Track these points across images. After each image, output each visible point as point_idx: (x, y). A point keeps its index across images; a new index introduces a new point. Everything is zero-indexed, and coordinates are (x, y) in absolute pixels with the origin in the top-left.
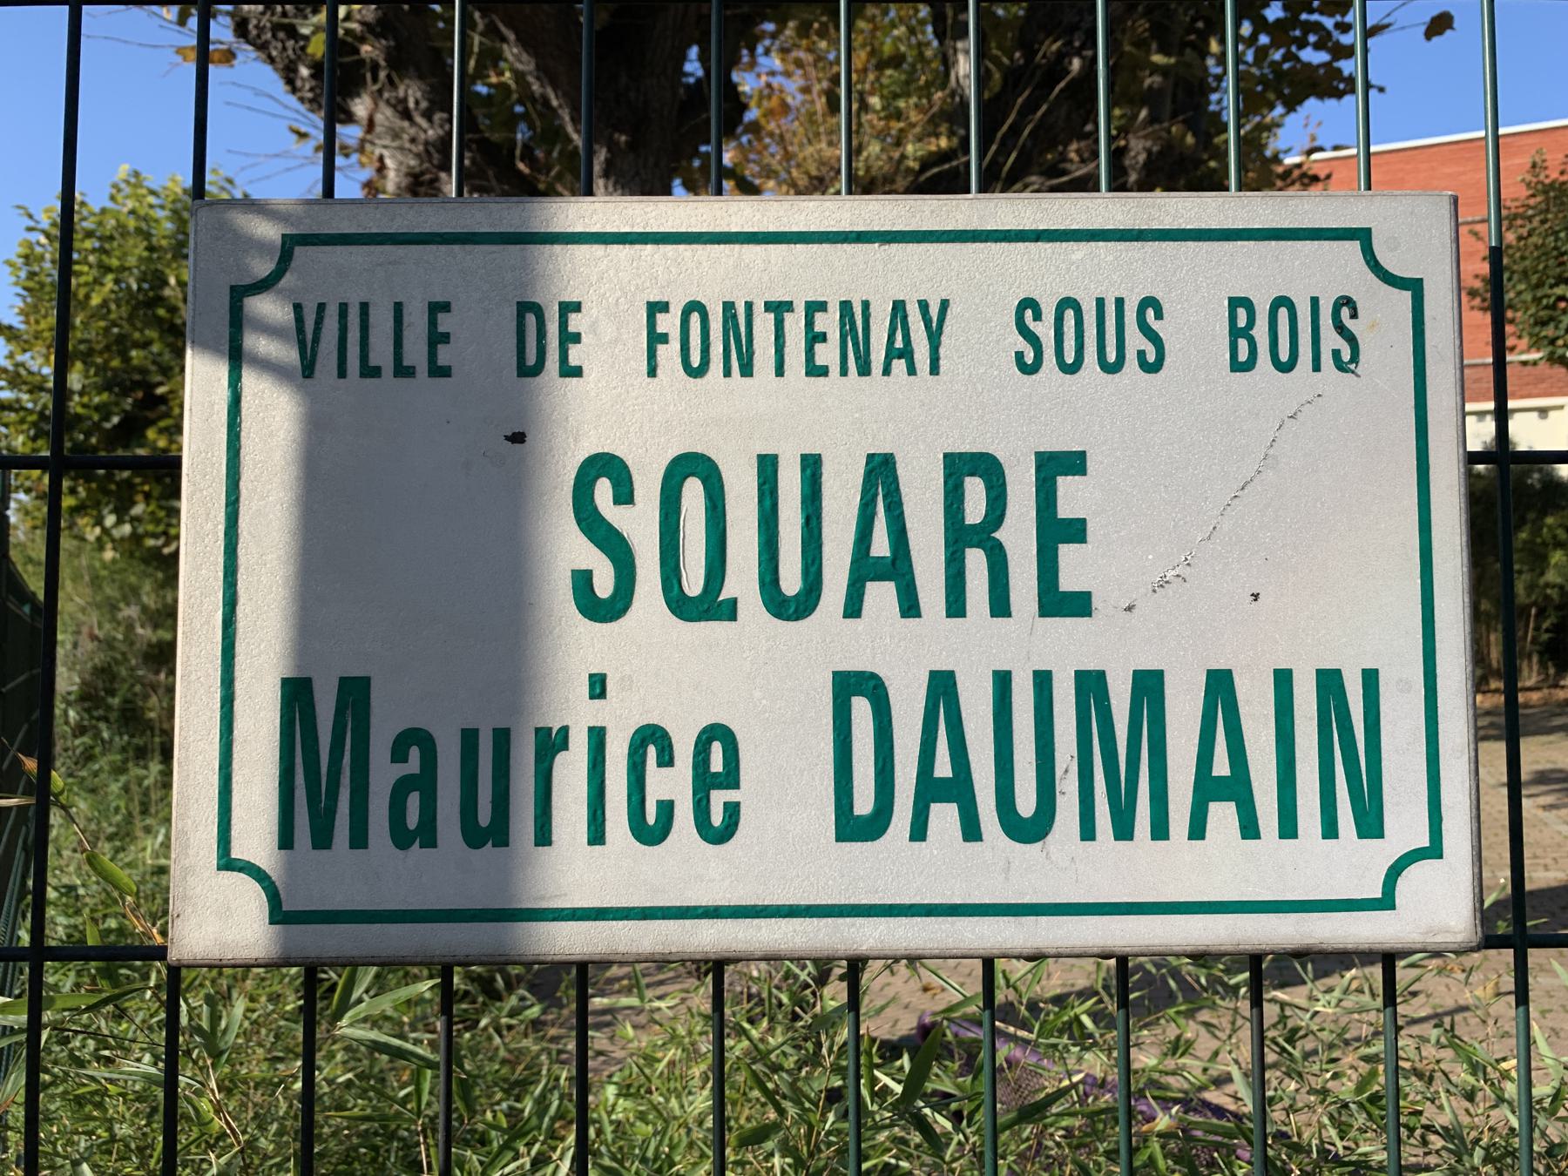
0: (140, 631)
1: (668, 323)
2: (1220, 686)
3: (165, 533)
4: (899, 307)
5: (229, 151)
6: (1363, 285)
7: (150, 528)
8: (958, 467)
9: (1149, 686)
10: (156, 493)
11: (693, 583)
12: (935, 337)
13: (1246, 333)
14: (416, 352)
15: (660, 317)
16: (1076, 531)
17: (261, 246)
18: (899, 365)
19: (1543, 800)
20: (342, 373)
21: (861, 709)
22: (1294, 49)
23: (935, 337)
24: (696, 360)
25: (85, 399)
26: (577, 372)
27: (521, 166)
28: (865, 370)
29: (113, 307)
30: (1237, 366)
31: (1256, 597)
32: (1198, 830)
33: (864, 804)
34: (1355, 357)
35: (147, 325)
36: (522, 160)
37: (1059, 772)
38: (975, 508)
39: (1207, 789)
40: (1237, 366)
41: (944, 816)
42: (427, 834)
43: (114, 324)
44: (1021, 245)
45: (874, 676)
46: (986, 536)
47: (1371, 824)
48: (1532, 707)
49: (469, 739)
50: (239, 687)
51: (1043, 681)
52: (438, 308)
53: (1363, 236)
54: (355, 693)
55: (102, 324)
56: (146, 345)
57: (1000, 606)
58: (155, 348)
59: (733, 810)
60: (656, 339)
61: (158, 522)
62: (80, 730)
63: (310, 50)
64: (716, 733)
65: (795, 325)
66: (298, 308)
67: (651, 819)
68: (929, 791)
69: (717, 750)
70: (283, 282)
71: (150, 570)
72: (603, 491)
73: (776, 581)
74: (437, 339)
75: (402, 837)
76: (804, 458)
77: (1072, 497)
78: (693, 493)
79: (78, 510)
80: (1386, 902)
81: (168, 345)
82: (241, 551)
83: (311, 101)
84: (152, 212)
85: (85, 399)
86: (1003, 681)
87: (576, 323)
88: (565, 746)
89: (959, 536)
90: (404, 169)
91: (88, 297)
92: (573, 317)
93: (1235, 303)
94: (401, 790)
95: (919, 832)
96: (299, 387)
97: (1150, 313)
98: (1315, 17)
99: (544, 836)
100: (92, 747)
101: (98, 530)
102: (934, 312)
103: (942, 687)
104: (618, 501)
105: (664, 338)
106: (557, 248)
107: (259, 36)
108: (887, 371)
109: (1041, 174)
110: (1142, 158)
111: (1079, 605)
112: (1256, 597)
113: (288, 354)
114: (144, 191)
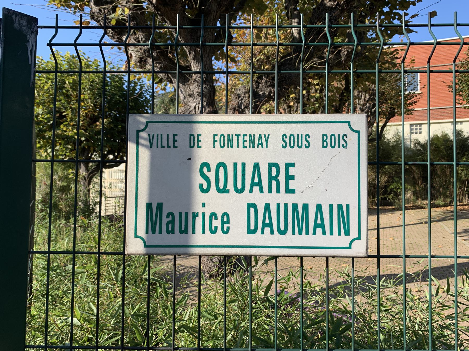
0: (58, 182)
1: (217, 138)
2: (319, 207)
3: (65, 155)
4: (260, 136)
6: (348, 132)
7: (61, 153)
8: (271, 165)
9: (306, 207)
10: (62, 143)
11: (221, 186)
12: (267, 141)
13: (326, 141)
14: (171, 143)
15: (216, 137)
16: (293, 178)
17: (142, 123)
18: (260, 146)
19: (464, 238)
20: (157, 147)
21: (252, 210)
22: (391, 20)
23: (267, 141)
24: (222, 145)
25: (43, 116)
26: (200, 147)
27: (170, 55)
28: (254, 147)
29: (51, 90)
30: (324, 147)
31: (326, 190)
32: (314, 233)
33: (252, 227)
34: (346, 146)
35: (60, 95)
36: (170, 53)
37: (288, 222)
38: (274, 173)
39: (316, 226)
40: (324, 147)
41: (267, 230)
42: (173, 231)
43: (51, 95)
44: (283, 124)
45: (255, 204)
46: (276, 178)
47: (347, 233)
48: (465, 210)
49: (181, 214)
50: (138, 204)
51: (286, 205)
52: (175, 135)
53: (349, 122)
54: (160, 206)
55: (48, 95)
56: (60, 101)
57: (278, 191)
58: (63, 101)
59: (228, 228)
60: (215, 141)
61: (63, 151)
62: (42, 211)
63: (111, 23)
64: (225, 214)
65: (241, 138)
66: (149, 135)
67: (213, 229)
68: (265, 225)
69: (225, 217)
70: (146, 130)
71: (60, 165)
72: (205, 169)
73: (237, 186)
74: (175, 141)
75: (168, 232)
76: (242, 163)
77: (292, 171)
78: (222, 169)
79: (40, 148)
80: (350, 247)
81: (66, 101)
82: (139, 180)
83: (111, 36)
84: (61, 62)
85: (43, 116)
86: (278, 205)
87: (200, 138)
88: (198, 216)
89: (271, 178)
90: (137, 56)
91: (43, 87)
92: (200, 137)
93: (324, 135)
94: (168, 223)
95: (262, 232)
96: (150, 149)
97: (307, 137)
98: (398, 11)
99: (194, 232)
100: (45, 216)
101: (46, 153)
102: (267, 136)
103: (267, 206)
104: (208, 171)
105: (217, 141)
106: (197, 124)
107: (97, 19)
108: (258, 147)
109: (317, 58)
110: (346, 53)
111: (293, 191)
112: (326, 190)
113: (147, 143)
114: (59, 56)
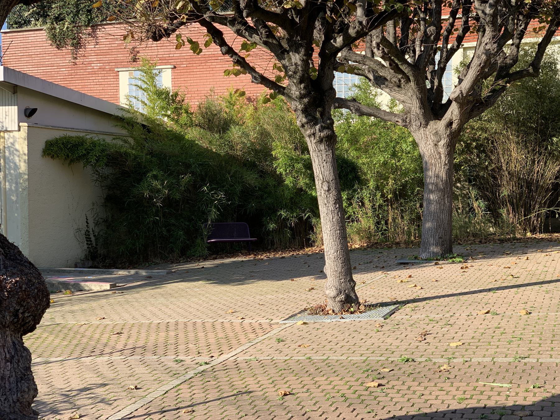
5: (393, 370)
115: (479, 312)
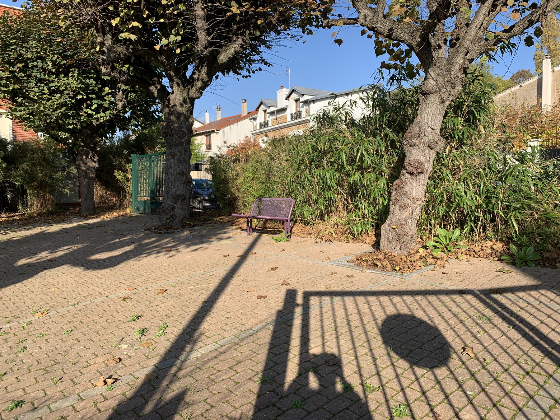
115: (95, 289)
